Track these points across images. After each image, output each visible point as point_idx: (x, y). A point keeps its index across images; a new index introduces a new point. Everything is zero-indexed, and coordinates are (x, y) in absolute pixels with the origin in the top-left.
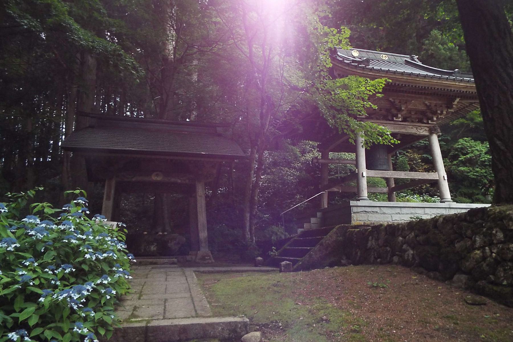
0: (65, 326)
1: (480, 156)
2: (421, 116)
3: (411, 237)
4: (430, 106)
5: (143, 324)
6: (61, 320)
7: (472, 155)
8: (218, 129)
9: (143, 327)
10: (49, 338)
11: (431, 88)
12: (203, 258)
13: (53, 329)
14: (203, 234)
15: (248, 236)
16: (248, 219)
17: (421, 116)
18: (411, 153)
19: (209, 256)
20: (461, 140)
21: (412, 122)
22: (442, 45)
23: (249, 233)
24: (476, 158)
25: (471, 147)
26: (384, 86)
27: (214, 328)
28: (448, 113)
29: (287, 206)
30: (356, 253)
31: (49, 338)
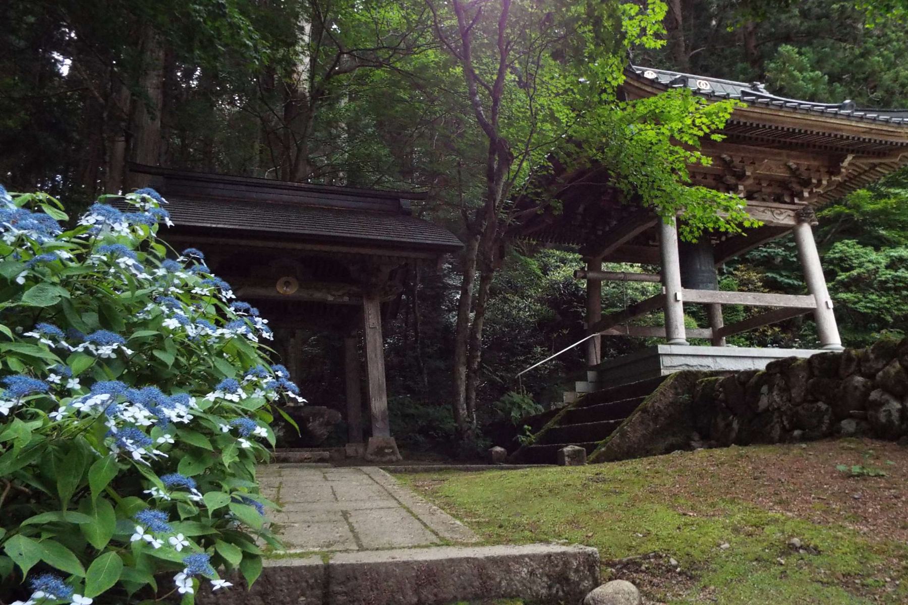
0: (98, 528)
1: (876, 271)
2: (778, 191)
3: (892, 371)
4: (797, 169)
5: (316, 561)
6: (81, 499)
7: (862, 270)
8: (403, 201)
9: (317, 567)
10: (25, 568)
11: (806, 131)
12: (380, 451)
13: (45, 536)
14: (379, 404)
15: (463, 412)
16: (463, 377)
17: (778, 191)
18: (742, 271)
19: (391, 448)
20: (839, 246)
21: (764, 200)
22: (801, 72)
23: (465, 406)
24: (870, 276)
25: (858, 256)
26: (728, 116)
27: (508, 571)
28: (830, 183)
29: (518, 366)
30: (729, 425)
31: (25, 568)
